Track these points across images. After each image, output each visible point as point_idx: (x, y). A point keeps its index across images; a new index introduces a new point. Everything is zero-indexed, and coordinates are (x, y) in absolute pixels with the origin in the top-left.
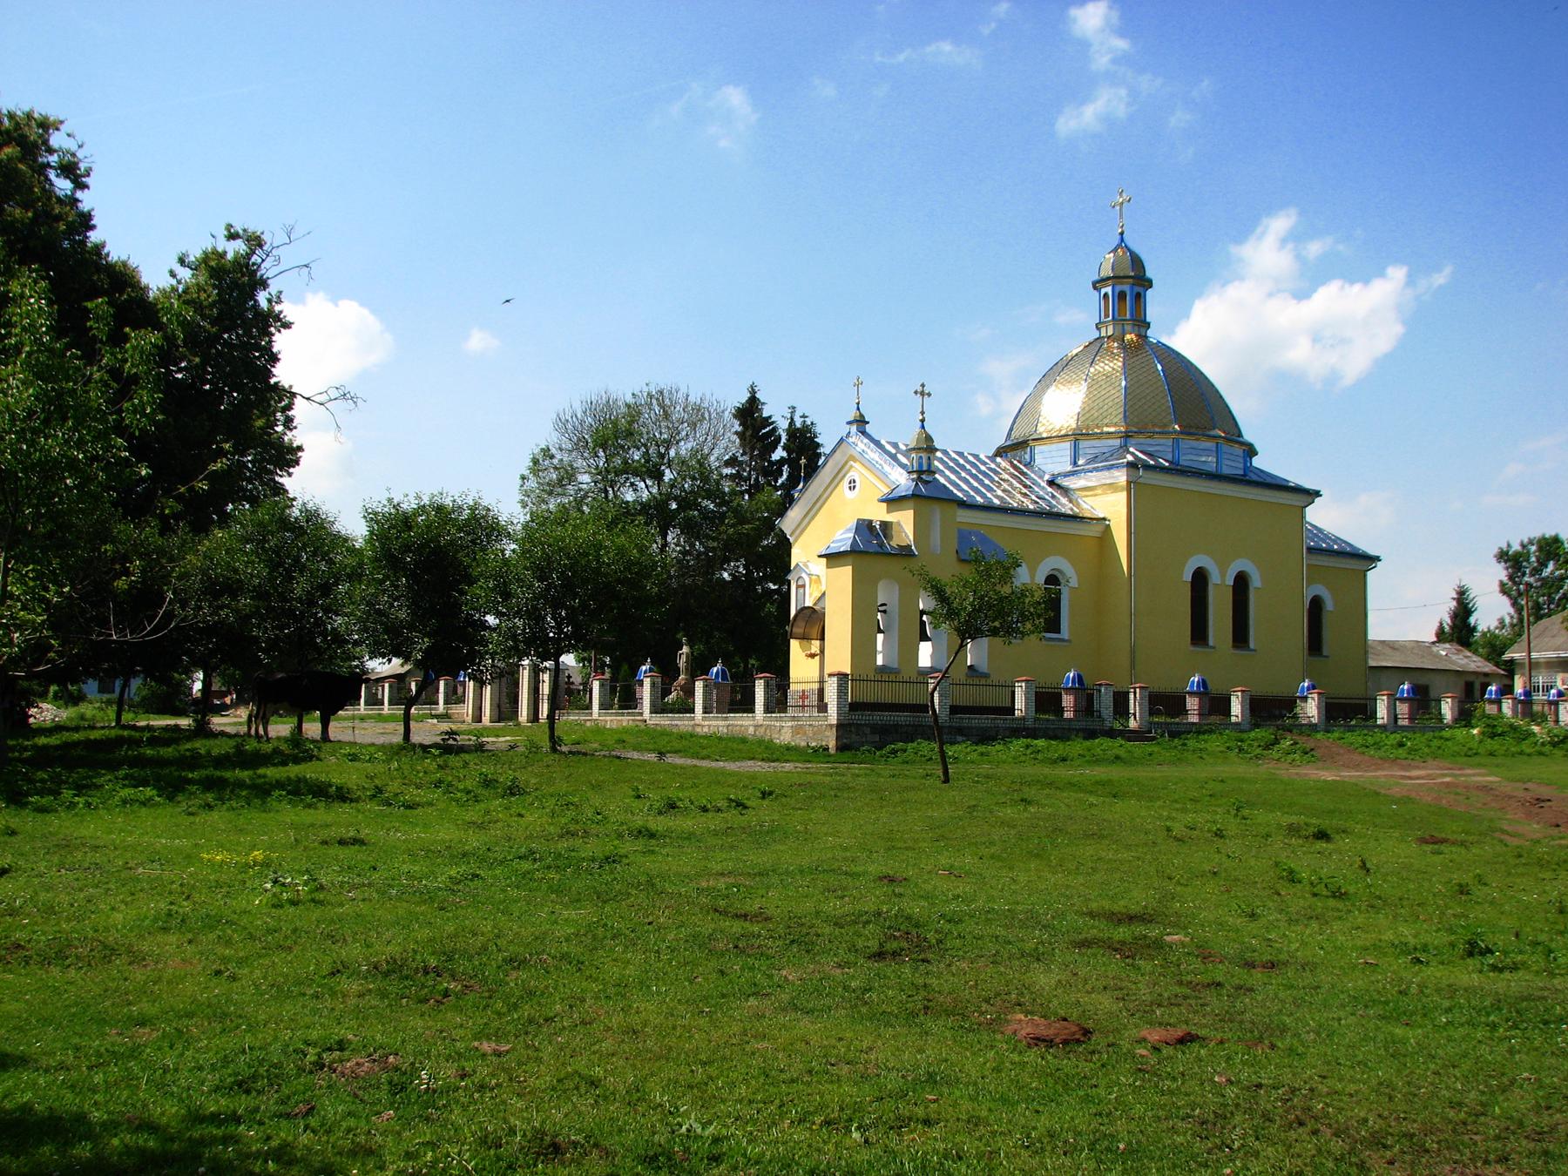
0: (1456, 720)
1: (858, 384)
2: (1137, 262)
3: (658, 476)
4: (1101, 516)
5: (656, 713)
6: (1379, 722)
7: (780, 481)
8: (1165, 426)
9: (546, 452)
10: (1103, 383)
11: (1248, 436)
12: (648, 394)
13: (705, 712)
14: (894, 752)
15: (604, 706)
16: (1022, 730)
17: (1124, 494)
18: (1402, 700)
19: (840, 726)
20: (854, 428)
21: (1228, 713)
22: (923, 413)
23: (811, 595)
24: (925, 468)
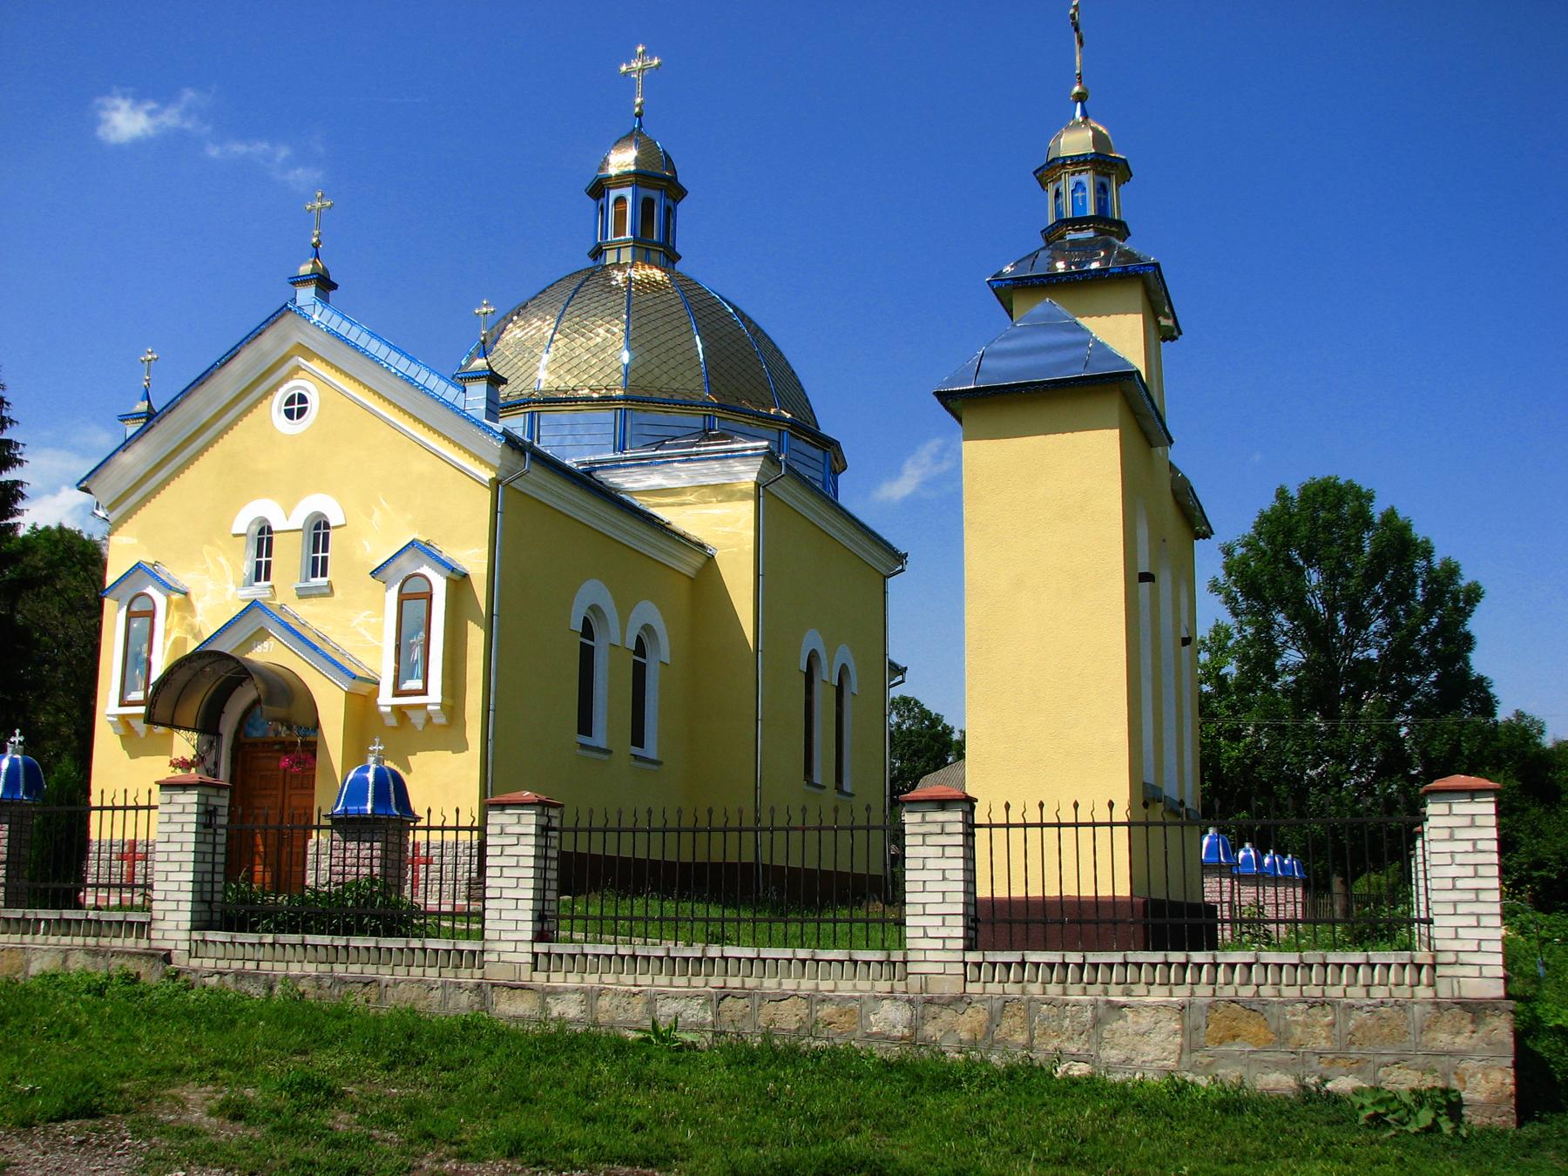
17: (750, 505)
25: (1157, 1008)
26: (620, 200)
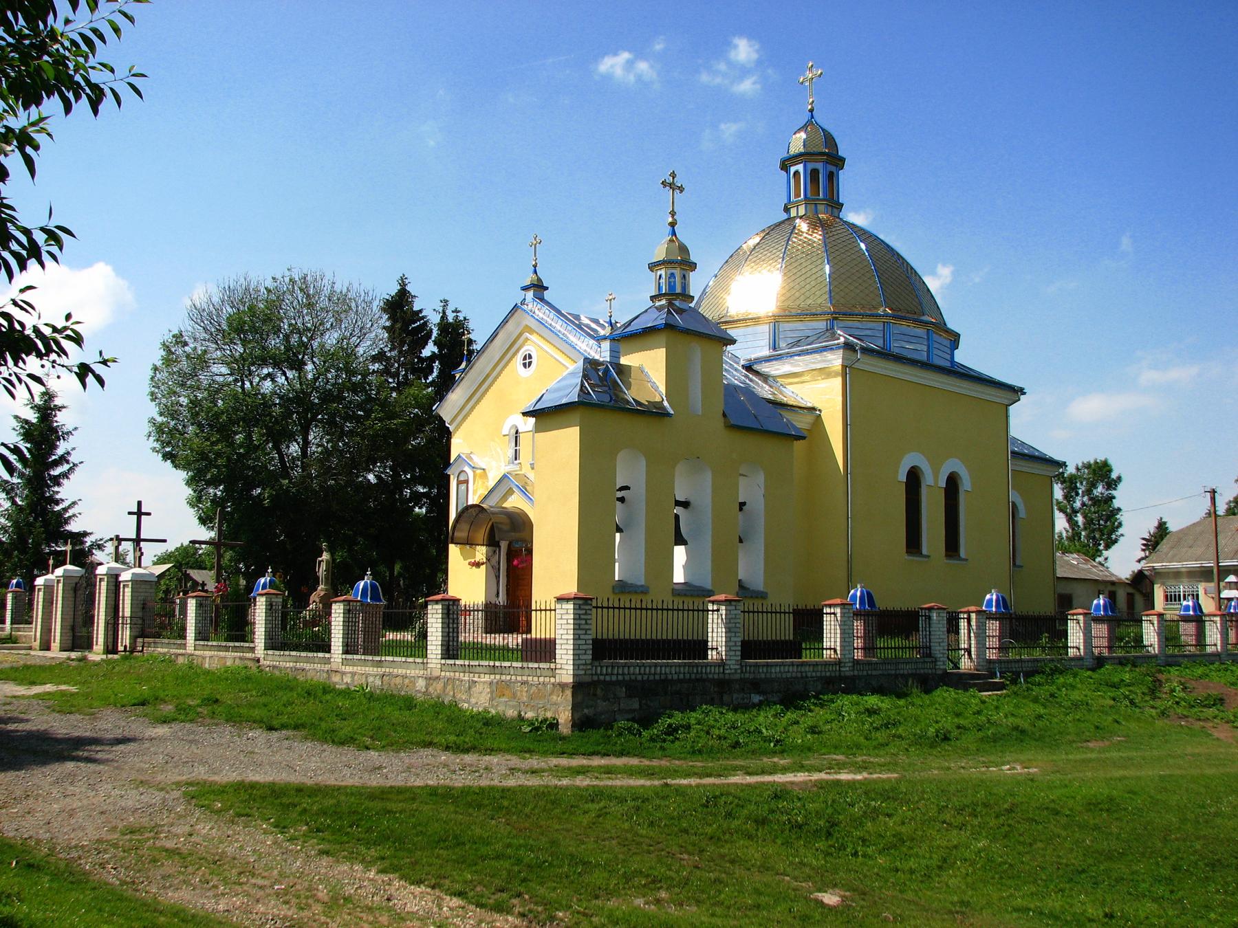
2: (830, 140)
3: (299, 366)
5: (273, 648)
7: (430, 379)
9: (179, 339)
10: (803, 260)
11: (951, 325)
12: (291, 280)
13: (346, 652)
14: (672, 730)
15: (201, 635)
17: (838, 381)
19: (579, 687)
20: (530, 294)
22: (673, 214)
23: (475, 492)
24: (678, 290)
25: (485, 682)
26: (797, 173)
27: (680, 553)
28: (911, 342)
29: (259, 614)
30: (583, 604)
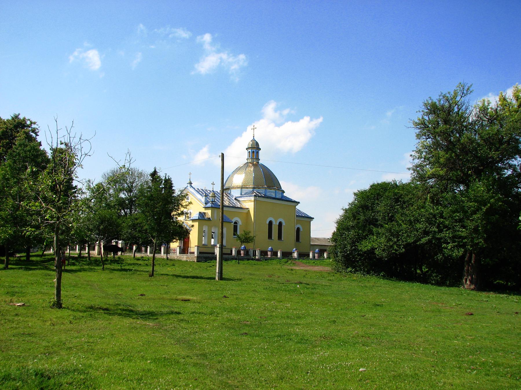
0: (327, 258)
1: (190, 174)
2: (257, 144)
4: (247, 208)
6: (310, 258)
8: (263, 186)
11: (283, 188)
16: (234, 258)
17: (253, 203)
18: (316, 253)
19: (197, 257)
20: (189, 185)
21: (277, 255)
27: (213, 240)
28: (271, 193)
29: (162, 249)
30: (198, 247)
